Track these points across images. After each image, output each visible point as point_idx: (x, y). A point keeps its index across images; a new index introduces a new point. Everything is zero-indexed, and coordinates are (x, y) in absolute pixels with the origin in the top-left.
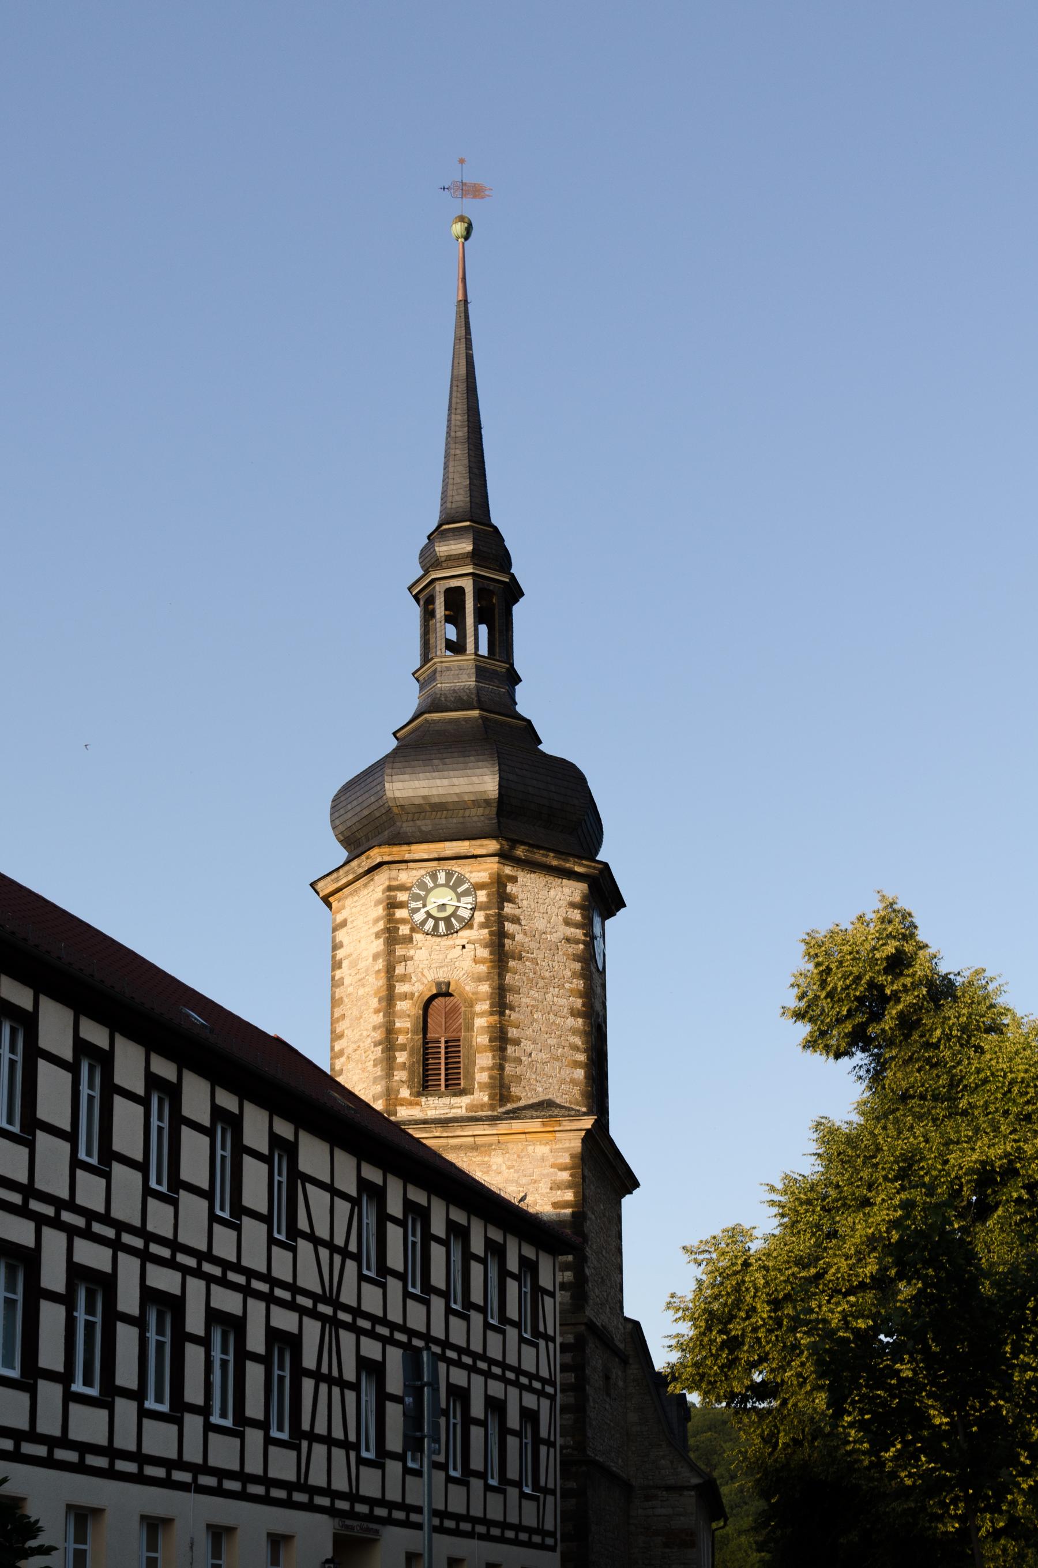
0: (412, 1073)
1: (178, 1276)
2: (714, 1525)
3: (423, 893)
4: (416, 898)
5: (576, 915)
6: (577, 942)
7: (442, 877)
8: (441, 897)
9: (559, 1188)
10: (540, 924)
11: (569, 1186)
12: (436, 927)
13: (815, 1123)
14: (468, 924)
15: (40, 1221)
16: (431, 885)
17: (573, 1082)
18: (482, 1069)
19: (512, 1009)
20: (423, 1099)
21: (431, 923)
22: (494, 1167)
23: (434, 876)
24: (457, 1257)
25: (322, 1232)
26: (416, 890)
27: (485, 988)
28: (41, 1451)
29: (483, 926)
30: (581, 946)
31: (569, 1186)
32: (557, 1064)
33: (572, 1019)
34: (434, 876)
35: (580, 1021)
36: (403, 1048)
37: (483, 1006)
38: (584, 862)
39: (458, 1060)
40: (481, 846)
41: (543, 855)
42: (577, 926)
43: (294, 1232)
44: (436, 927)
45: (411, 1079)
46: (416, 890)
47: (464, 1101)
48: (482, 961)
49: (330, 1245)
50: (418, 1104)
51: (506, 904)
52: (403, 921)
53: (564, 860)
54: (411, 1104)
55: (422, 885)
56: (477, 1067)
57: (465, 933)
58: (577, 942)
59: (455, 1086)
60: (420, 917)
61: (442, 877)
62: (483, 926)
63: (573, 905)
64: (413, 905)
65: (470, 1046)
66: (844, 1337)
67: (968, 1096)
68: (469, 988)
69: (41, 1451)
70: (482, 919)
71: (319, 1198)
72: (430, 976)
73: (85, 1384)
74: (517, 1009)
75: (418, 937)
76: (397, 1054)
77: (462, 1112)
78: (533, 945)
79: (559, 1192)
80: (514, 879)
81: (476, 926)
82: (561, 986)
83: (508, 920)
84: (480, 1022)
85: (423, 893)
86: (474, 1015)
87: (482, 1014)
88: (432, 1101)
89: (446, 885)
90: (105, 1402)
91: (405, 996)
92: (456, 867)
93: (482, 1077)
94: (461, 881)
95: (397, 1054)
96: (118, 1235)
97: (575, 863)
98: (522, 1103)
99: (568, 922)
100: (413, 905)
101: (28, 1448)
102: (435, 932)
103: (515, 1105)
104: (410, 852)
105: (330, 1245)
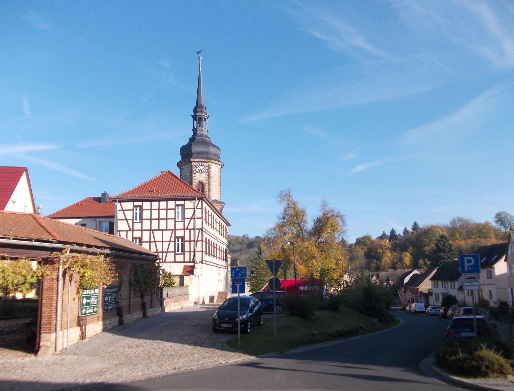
2: (32, 295)
5: (219, 171)
8: (201, 168)
13: (277, 229)
14: (205, 172)
26: (197, 166)
27: (207, 182)
29: (207, 172)
33: (457, 298)
34: (199, 164)
39: (436, 287)
46: (197, 166)
55: (198, 165)
57: (204, 173)
61: (201, 164)
62: (207, 172)
63: (219, 169)
64: (196, 168)
66: (447, 262)
67: (110, 274)
68: (205, 182)
72: (199, 180)
75: (197, 173)
78: (214, 176)
80: (211, 165)
92: (203, 163)
94: (203, 165)
99: (218, 172)
100: (196, 168)
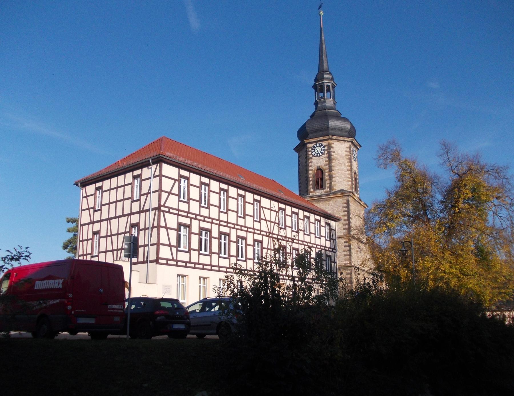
0: (313, 186)
1: (229, 229)
3: (314, 148)
4: (313, 149)
6: (348, 155)
7: (318, 145)
9: (344, 208)
10: (340, 152)
11: (99, 191)
12: (317, 155)
15: (191, 218)
16: (316, 146)
17: (348, 185)
18: (327, 184)
19: (333, 170)
20: (316, 191)
21: (316, 154)
22: (331, 204)
23: (316, 145)
24: (307, 223)
25: (268, 218)
26: (313, 148)
27: (328, 167)
28: (193, 265)
29: (327, 154)
30: (349, 156)
31: (99, 191)
32: (344, 181)
35: (350, 172)
36: (311, 181)
37: (328, 171)
38: (349, 138)
40: (325, 137)
41: (339, 138)
42: (348, 152)
43: (260, 219)
44: (317, 155)
45: (313, 187)
46: (313, 148)
47: (325, 190)
48: (327, 161)
49: (271, 222)
50: (314, 192)
51: (331, 149)
52: (310, 155)
53: (344, 138)
54: (313, 192)
55: (314, 147)
56: (326, 183)
58: (348, 155)
59: (322, 187)
60: (314, 153)
61: (318, 145)
64: (312, 151)
65: (325, 179)
68: (324, 167)
69: (193, 265)
70: (327, 152)
71: (268, 212)
72: (317, 165)
73: (224, 254)
74: (335, 171)
75: (313, 157)
76: (310, 182)
77: (324, 193)
79: (344, 209)
81: (325, 154)
82: (345, 165)
83: (332, 152)
84: (327, 174)
85: (314, 148)
86: (325, 173)
87: (327, 172)
88: (318, 191)
89: (319, 146)
90: (189, 252)
91: (311, 170)
93: (327, 185)
94: (322, 145)
95: (310, 182)
96: (212, 221)
97: (347, 139)
98: (336, 190)
99: (346, 151)
100: (312, 151)
101: (197, 266)
102: (317, 156)
103: (335, 191)
104: (311, 140)
105: (271, 222)
